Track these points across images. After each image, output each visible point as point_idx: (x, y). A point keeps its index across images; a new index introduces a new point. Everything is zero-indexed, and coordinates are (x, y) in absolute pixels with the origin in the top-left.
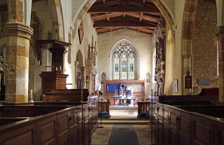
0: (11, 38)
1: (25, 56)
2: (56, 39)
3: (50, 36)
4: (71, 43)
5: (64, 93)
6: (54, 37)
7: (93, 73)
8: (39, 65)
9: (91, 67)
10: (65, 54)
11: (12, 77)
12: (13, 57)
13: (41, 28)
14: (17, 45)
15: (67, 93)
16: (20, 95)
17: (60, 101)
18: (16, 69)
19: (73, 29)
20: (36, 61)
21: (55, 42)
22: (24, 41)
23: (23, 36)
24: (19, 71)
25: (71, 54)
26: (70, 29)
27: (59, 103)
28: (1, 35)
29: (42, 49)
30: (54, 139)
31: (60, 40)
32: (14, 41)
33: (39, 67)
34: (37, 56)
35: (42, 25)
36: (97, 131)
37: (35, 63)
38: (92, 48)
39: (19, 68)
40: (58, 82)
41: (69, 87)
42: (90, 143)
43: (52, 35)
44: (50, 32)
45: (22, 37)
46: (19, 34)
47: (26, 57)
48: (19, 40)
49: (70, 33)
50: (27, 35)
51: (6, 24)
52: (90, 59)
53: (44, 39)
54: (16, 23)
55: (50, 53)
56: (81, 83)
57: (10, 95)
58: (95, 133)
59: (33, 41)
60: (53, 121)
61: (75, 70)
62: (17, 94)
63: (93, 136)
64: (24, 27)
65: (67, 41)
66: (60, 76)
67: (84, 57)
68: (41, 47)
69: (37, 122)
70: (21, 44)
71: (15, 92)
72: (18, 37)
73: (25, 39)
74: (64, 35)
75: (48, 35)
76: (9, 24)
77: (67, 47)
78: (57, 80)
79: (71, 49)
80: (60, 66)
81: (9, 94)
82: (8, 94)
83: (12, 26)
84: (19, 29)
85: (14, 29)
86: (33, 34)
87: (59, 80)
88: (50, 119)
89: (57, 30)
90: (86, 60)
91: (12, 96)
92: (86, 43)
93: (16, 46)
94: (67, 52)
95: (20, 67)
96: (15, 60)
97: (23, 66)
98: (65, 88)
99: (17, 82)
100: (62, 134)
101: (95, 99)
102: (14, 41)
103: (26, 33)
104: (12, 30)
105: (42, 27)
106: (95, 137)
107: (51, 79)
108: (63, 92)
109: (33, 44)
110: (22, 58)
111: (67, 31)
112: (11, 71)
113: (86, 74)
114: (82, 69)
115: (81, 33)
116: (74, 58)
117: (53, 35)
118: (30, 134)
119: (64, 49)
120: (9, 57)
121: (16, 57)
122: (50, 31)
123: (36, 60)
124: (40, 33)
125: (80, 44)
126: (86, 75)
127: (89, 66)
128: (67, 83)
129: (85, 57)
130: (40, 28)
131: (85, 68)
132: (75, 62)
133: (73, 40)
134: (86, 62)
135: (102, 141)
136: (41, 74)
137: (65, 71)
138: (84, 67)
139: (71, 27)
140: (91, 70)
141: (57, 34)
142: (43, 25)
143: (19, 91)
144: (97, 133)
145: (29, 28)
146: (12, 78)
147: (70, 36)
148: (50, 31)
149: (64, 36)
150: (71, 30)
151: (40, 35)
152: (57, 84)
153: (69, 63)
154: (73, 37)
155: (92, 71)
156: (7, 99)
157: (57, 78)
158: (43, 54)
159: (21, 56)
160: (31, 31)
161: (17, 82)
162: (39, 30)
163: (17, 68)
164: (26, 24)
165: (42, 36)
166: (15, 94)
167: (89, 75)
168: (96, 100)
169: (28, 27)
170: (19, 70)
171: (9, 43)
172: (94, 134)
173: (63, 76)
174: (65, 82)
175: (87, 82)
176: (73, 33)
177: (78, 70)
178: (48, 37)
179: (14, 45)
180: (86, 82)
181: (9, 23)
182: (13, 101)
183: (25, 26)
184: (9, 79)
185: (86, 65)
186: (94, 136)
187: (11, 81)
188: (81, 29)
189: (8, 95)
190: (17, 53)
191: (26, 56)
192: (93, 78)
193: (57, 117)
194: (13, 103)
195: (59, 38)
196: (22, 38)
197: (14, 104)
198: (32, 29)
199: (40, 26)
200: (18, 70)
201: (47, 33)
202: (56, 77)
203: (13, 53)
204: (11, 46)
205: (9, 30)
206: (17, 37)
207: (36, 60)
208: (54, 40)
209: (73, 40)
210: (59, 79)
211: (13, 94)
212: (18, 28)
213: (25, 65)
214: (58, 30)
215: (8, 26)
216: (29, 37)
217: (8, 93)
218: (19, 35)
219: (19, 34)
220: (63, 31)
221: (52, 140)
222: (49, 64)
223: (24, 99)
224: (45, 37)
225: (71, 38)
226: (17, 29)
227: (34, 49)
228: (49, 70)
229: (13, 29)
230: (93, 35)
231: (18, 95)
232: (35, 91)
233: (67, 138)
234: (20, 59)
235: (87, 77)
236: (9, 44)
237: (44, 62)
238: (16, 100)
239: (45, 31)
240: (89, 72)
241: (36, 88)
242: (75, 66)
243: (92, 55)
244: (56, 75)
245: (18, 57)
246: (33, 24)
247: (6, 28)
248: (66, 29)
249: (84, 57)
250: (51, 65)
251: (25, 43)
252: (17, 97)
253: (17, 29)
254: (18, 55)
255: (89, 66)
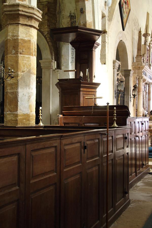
0: (10, 28)
1: (30, 55)
2: (81, 26)
3: (72, 20)
4: (107, 30)
5: (89, 112)
6: (78, 22)
7: (147, 80)
8: (55, 68)
9: (143, 69)
10: (96, 48)
11: (13, 87)
12: (14, 57)
13: (59, 7)
14: (19, 38)
15: (95, 112)
16: (24, 115)
17: (84, 125)
18: (18, 75)
19: (110, 5)
20: (52, 63)
21: (78, 30)
22: (29, 31)
23: (27, 23)
24: (21, 78)
25: (105, 49)
26: (105, 5)
27: (83, 127)
28: (2, 24)
29: (61, 42)
30: (55, 174)
31: (88, 27)
32: (14, 32)
33: (55, 72)
34: (53, 55)
35: (61, 3)
36: (146, 179)
37: (51, 66)
38: (146, 35)
39: (22, 74)
40: (84, 95)
41: (101, 103)
42: (127, 195)
43: (76, 19)
44: (74, 13)
45: (26, 25)
46: (22, 21)
47: (31, 57)
48: (22, 29)
49: (104, 12)
50: (33, 21)
51: (3, 5)
52: (141, 55)
53: (64, 26)
54: (17, 4)
55: (73, 49)
56: (124, 98)
57: (10, 114)
58: (141, 183)
59: (48, 31)
60: (53, 147)
61: (114, 76)
62: (19, 112)
63: (136, 186)
64: (28, 9)
65: (98, 27)
66: (87, 85)
67: (131, 52)
68: (60, 40)
69: (26, 145)
70: (24, 36)
71: (17, 110)
72: (20, 25)
73: (29, 29)
74: (94, 18)
75: (71, 19)
76: (7, 5)
77: (98, 37)
78: (81, 93)
79: (107, 41)
80: (87, 70)
81: (9, 112)
82: (7, 113)
83: (10, 9)
84: (20, 12)
85: (14, 14)
86: (41, 19)
87: (85, 93)
88: (49, 142)
89: (82, 9)
90: (135, 59)
91: (12, 115)
92: (134, 28)
93: (18, 39)
94: (98, 45)
95: (23, 72)
96: (17, 62)
97: (28, 70)
98: (95, 104)
99: (19, 95)
100: (69, 169)
101: (143, 124)
102: (15, 33)
103: (30, 18)
104: (12, 14)
105: (61, 6)
106: (139, 188)
107: (74, 90)
108: (89, 111)
109: (48, 35)
110: (26, 58)
111: (99, 9)
112: (8, 77)
113: (134, 81)
114: (127, 73)
115: (125, 10)
116: (111, 55)
117: (76, 19)
118: (15, 158)
119: (94, 41)
120: (9, 58)
121: (17, 57)
122: (73, 12)
123: (52, 61)
124: (57, 16)
125: (123, 30)
126: (134, 84)
127: (139, 67)
128: (81, 90)
129: (133, 52)
130: (58, 8)
131: (132, 72)
132: (114, 62)
133: (109, 25)
134: (135, 61)
135: (149, 195)
136: (58, 82)
137: (94, 77)
138: (130, 70)
139: (106, 2)
140: (143, 75)
141: (82, 16)
142: (62, 4)
143: (22, 108)
144: (144, 183)
145: (34, 10)
146: (12, 88)
147: (105, 18)
148: (73, 12)
149: (95, 20)
150: (107, 8)
151: (58, 19)
152: (82, 99)
153: (102, 64)
154: (110, 20)
155: (144, 77)
156: (6, 120)
157: (82, 89)
158: (64, 51)
159: (24, 54)
160: (39, 14)
161: (20, 95)
162: (57, 12)
163: (19, 73)
164: (31, 4)
165: (61, 21)
166: (17, 112)
167: (139, 84)
168: (144, 125)
169: (33, 8)
170: (23, 77)
171: (7, 36)
172: (139, 184)
173: (93, 86)
174: (95, 95)
175: (134, 95)
176: (109, 12)
177: (119, 75)
178: (70, 23)
179: (15, 38)
180: (133, 96)
181: (7, 4)
182: (14, 123)
183: (29, 8)
184: (9, 91)
185: (133, 67)
186: (139, 186)
187: (11, 93)
188: (126, 3)
189: (7, 114)
190: (20, 50)
191: (33, 54)
192: (147, 88)
193: (60, 142)
194: (15, 126)
195: (85, 24)
196: (26, 27)
197: (15, 127)
198: (39, 12)
199: (58, 5)
200: (20, 77)
201: (69, 15)
202: (80, 87)
203: (14, 52)
204: (11, 39)
205: (6, 15)
206: (18, 25)
207: (52, 61)
208: (77, 27)
209: (110, 24)
210: (85, 90)
211: (14, 113)
212: (19, 10)
213: (30, 69)
214: (83, 10)
215: (5, 9)
216: (36, 24)
217: (8, 111)
218: (22, 23)
219: (22, 21)
220: (92, 10)
221: (51, 175)
222: (71, 66)
223: (29, 121)
224: (65, 23)
225: (107, 22)
226: (17, 12)
227: (50, 43)
228: (72, 76)
229: (13, 12)
230: (149, 12)
231: (21, 114)
232: (51, 110)
233: (78, 176)
234: (23, 59)
235: (135, 87)
236: (9, 38)
237: (64, 64)
238: (18, 122)
239: (66, 13)
240: (139, 78)
241: (52, 106)
242: (114, 68)
243: (145, 47)
244: (80, 83)
245: (21, 56)
246: (47, 3)
247: (4, 12)
248: (98, 6)
249: (131, 52)
250: (74, 69)
251: (30, 34)
252: (19, 118)
253: (17, 12)
254: (20, 54)
255: (138, 67)
